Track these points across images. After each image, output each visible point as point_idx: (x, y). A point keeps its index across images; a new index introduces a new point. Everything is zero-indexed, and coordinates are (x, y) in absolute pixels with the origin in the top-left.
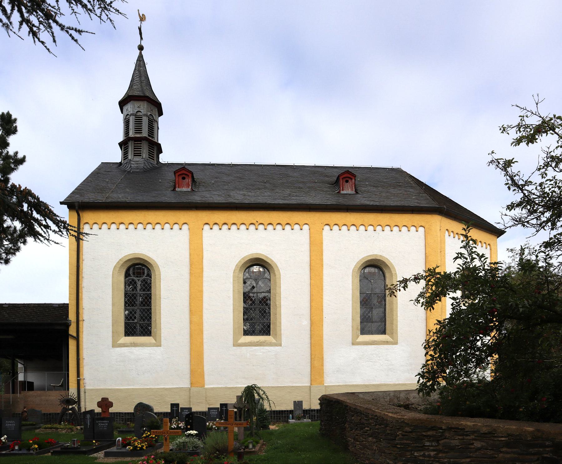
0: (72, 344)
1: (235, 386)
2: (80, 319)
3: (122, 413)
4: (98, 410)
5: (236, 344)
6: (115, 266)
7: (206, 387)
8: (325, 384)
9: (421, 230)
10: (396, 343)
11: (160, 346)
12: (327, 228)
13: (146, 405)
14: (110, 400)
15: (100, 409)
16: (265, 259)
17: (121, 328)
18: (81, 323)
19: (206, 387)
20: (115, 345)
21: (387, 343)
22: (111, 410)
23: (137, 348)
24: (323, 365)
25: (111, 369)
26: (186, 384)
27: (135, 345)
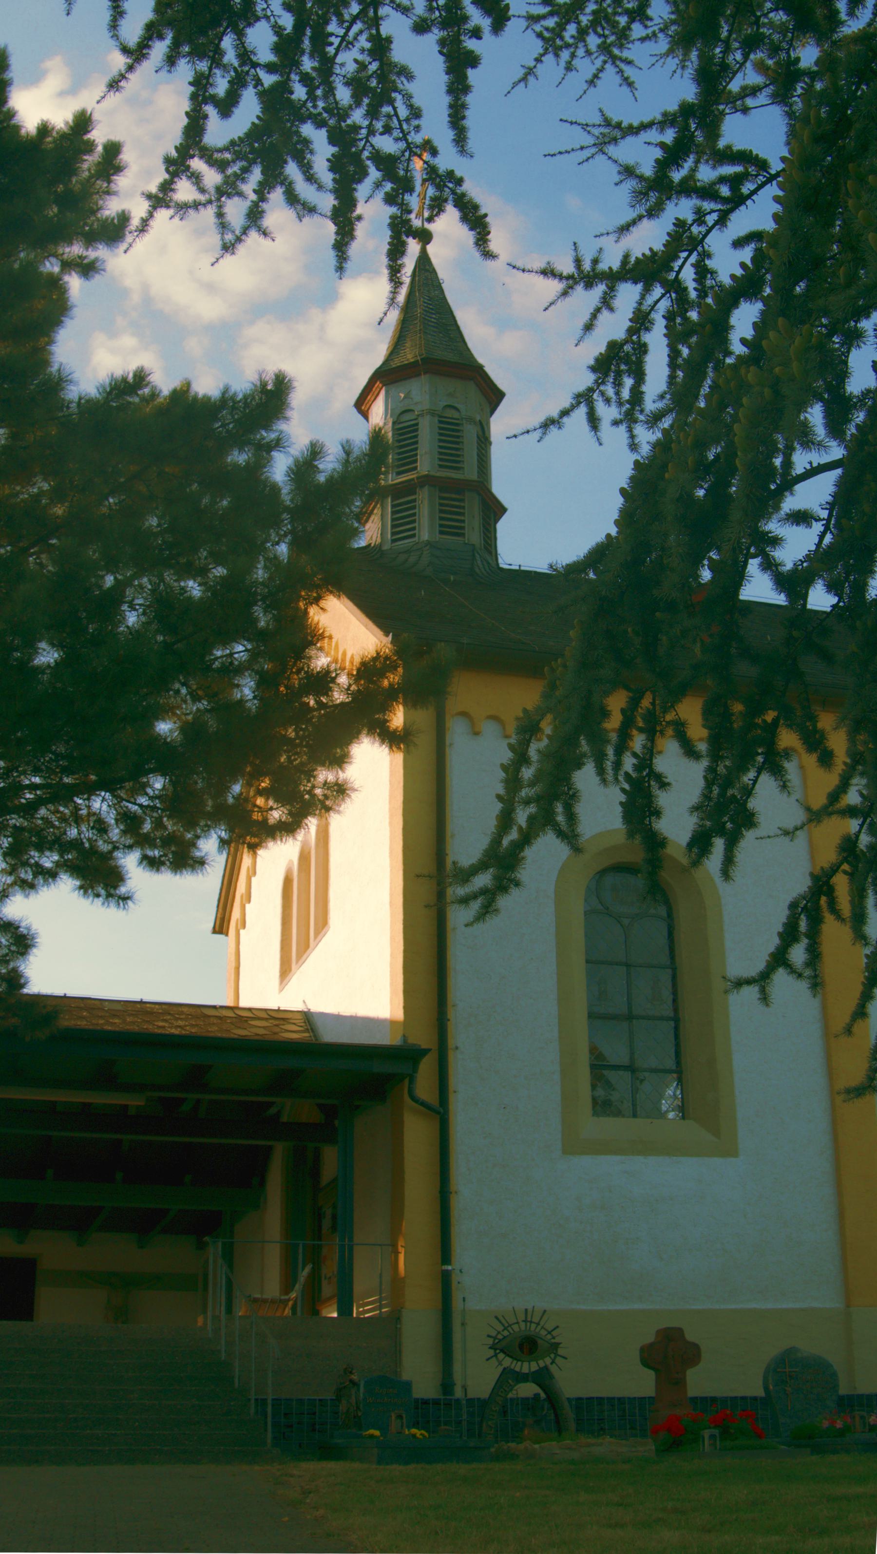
0: (416, 1133)
2: (451, 1043)
4: (642, 1383)
14: (690, 1337)
18: (451, 1056)
20: (574, 1145)
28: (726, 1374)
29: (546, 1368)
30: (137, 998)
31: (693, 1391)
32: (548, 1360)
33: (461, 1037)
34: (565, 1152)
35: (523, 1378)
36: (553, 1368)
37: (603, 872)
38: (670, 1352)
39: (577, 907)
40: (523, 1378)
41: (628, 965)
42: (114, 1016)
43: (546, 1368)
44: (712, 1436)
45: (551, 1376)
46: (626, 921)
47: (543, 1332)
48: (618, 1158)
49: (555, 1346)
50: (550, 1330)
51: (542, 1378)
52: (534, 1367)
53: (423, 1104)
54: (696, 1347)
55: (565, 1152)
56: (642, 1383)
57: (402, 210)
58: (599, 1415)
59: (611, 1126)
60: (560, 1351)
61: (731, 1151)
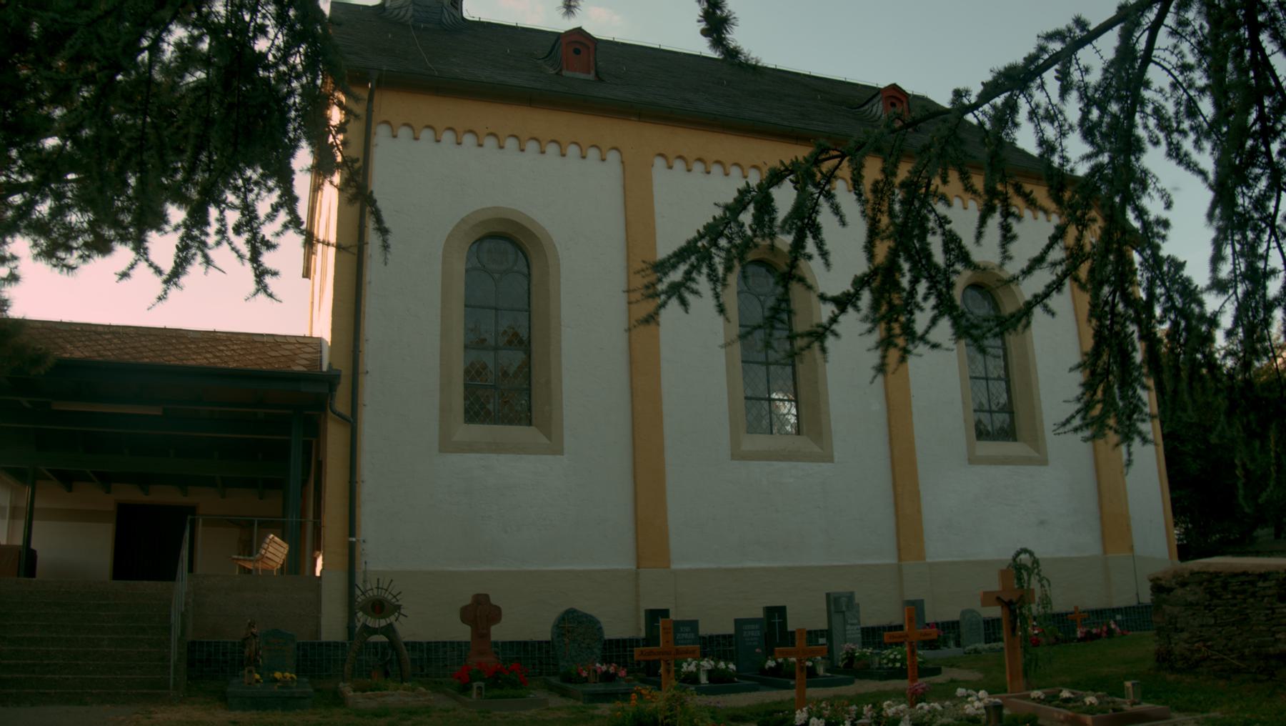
0: (334, 436)
1: (740, 566)
2: (361, 369)
3: (533, 643)
4: (463, 633)
5: (738, 455)
6: (451, 235)
7: (674, 566)
8: (928, 560)
9: (613, 157)
10: (1043, 462)
11: (561, 452)
12: (659, 162)
13: (586, 616)
14: (494, 601)
15: (468, 628)
16: (529, 226)
17: (458, 403)
18: (361, 378)
19: (674, 566)
20: (447, 445)
21: (1028, 461)
22: (499, 633)
23: (503, 457)
24: (919, 512)
25: (442, 517)
26: (626, 563)
27: (497, 447)
28: (525, 622)
29: (391, 625)
30: (211, 329)
31: (493, 638)
32: (392, 618)
33: (370, 361)
34: (440, 451)
35: (375, 631)
36: (396, 625)
37: (480, 240)
38: (481, 612)
39: (460, 267)
40: (375, 631)
41: (496, 309)
42: (192, 342)
43: (391, 625)
44: (479, 688)
45: (394, 631)
46: (497, 276)
47: (390, 597)
48: (478, 455)
49: (399, 607)
50: (984, 382)
51: (389, 630)
52: (383, 623)
53: (339, 415)
54: (498, 609)
55: (440, 451)
56: (463, 633)
57: (1063, 135)
58: (428, 662)
59: (479, 431)
60: (402, 611)
61: (558, 450)
